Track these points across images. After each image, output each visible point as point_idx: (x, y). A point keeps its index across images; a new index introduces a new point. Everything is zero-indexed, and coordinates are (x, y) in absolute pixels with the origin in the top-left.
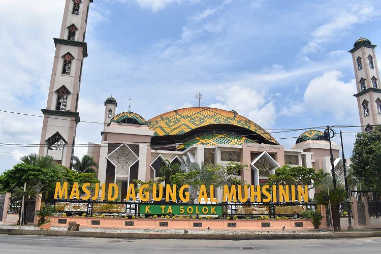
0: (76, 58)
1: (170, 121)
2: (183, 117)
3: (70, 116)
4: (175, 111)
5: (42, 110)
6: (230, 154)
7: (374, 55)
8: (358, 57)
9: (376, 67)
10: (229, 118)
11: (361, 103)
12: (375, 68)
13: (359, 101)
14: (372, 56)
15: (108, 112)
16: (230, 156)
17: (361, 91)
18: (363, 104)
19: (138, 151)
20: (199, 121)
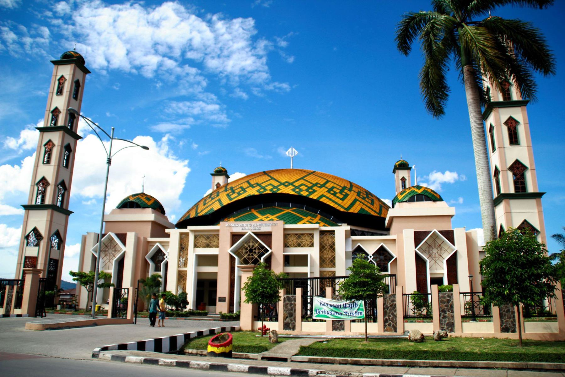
0: (529, 168)
1: (233, 192)
2: (281, 184)
3: (70, 64)
4: (265, 173)
5: (73, 212)
6: (208, 238)
7: (83, 83)
8: (62, 77)
9: (81, 101)
10: (316, 185)
11: (44, 143)
12: (78, 100)
13: (42, 138)
14: (81, 84)
15: (64, 150)
16: (208, 241)
17: (49, 125)
18: (45, 145)
19: (429, 231)
20: (307, 190)
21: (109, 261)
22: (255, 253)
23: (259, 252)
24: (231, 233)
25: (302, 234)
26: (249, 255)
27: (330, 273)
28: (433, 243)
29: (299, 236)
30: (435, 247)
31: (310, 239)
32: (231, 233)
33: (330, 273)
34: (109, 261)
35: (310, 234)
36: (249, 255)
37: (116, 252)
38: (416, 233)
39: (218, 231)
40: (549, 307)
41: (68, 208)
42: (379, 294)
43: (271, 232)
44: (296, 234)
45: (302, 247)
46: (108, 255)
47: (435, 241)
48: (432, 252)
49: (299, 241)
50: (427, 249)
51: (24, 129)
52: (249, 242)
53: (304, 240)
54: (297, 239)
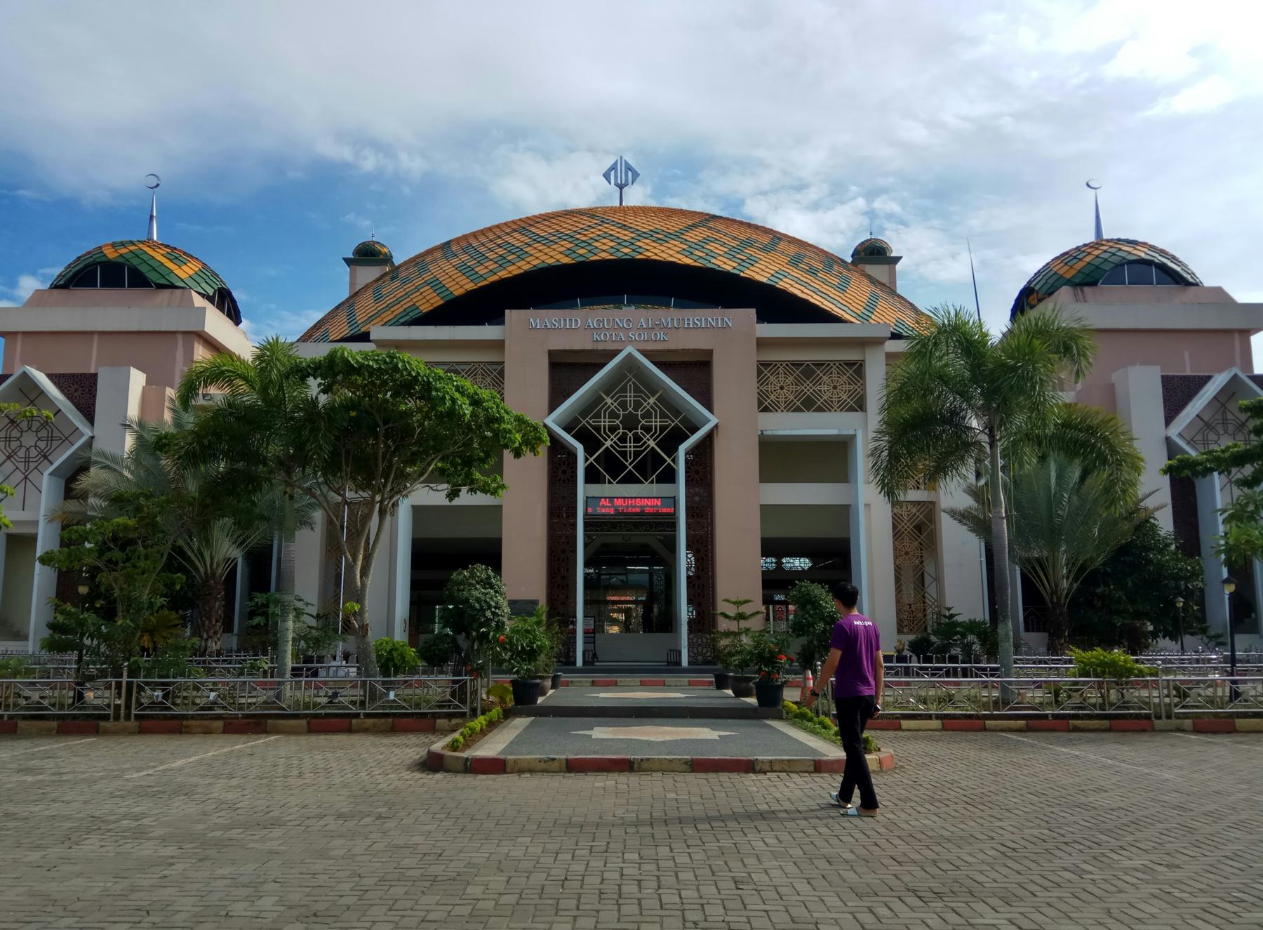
21: (26, 478)
22: (637, 405)
23: (663, 428)
24: (552, 354)
25: (819, 364)
26: (613, 415)
27: (914, 510)
28: (1219, 416)
29: (808, 371)
30: (1219, 435)
31: (851, 381)
32: (552, 354)
33: (914, 510)
34: (26, 478)
35: (850, 364)
36: (613, 415)
37: (55, 444)
38: (1167, 381)
39: (499, 345)
40: (1102, 707)
41: (6, 344)
42: (1255, 465)
43: (710, 352)
44: (797, 364)
45: (820, 409)
46: (21, 453)
47: (1224, 412)
48: (1215, 438)
49: (808, 388)
50: (1199, 437)
51: (110, 260)
52: (624, 390)
53: (825, 387)
54: (798, 382)
